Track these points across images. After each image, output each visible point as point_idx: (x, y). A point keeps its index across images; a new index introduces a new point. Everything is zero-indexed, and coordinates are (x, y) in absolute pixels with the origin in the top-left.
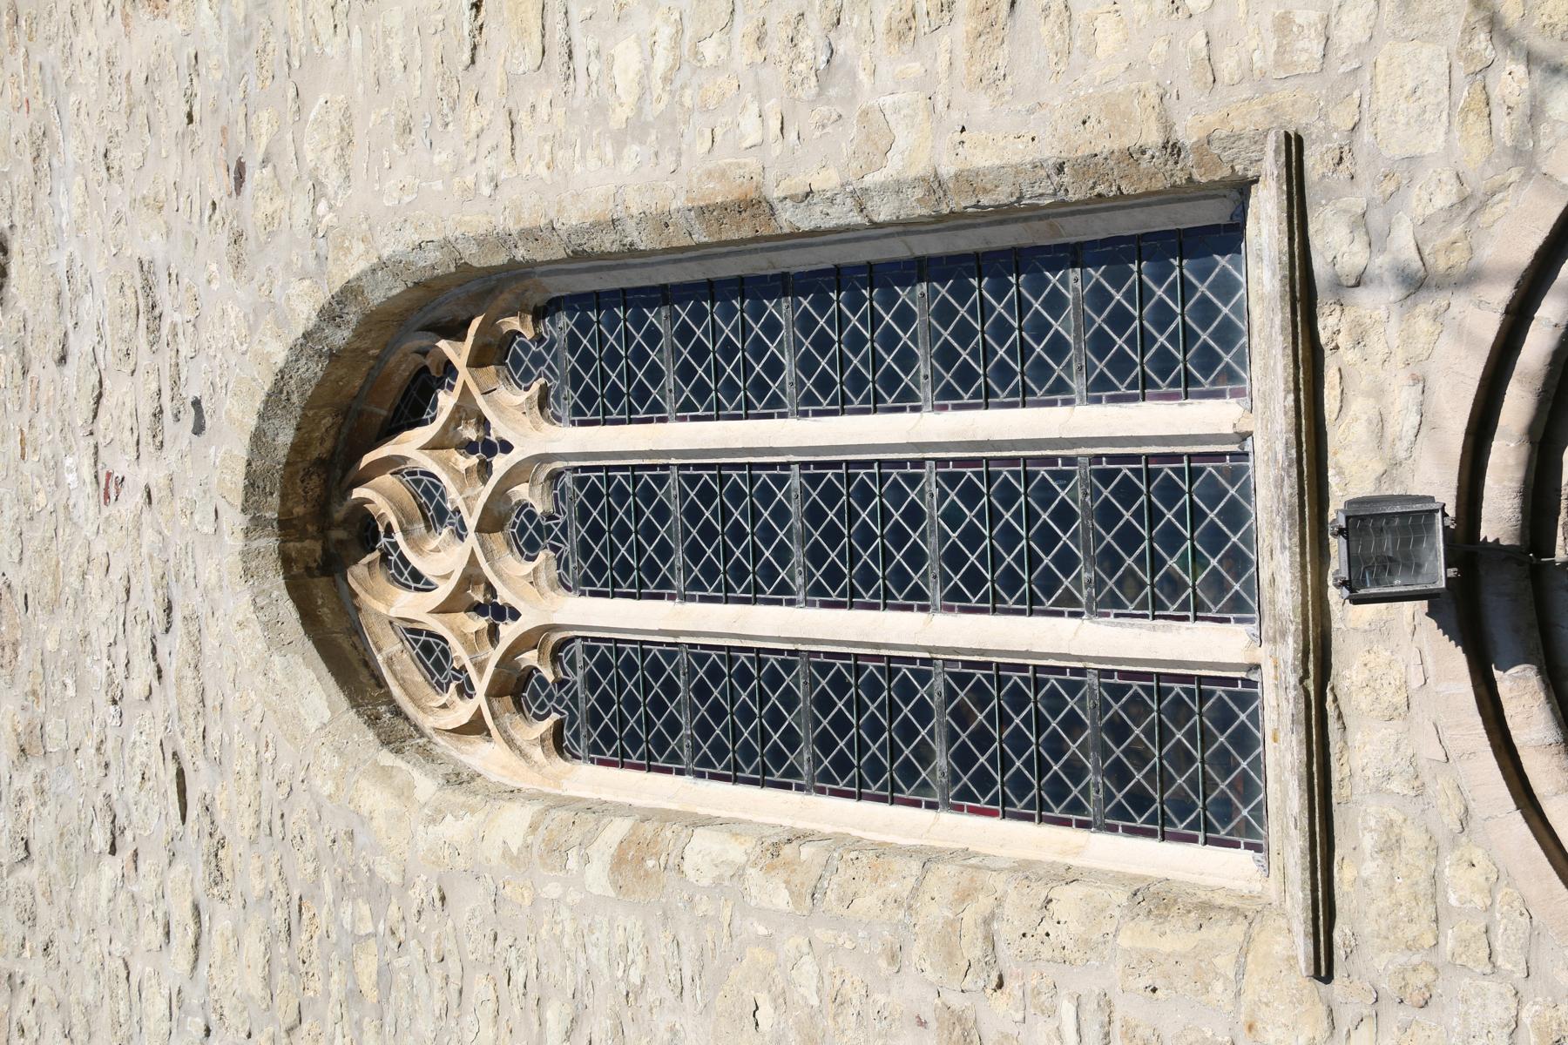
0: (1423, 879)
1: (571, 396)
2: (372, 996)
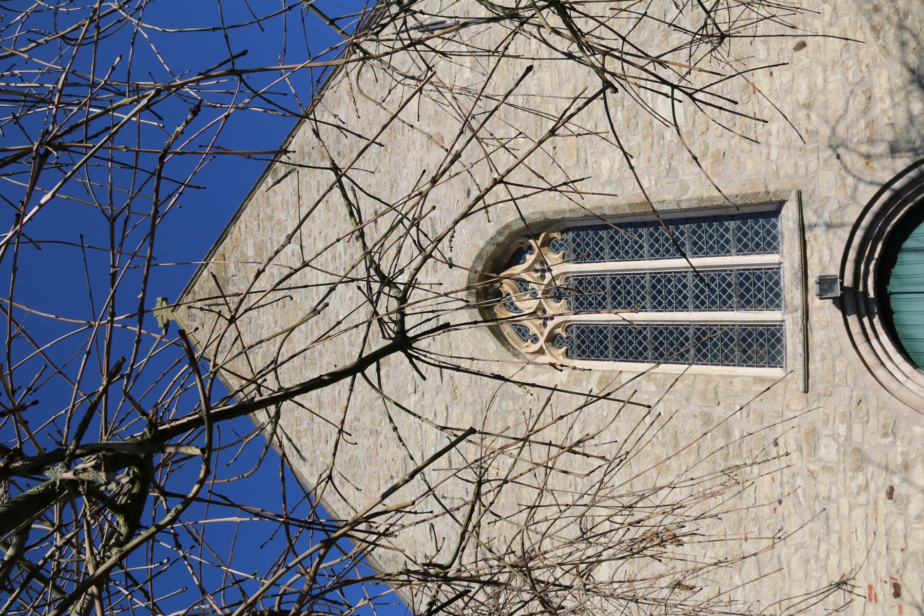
0: (830, 365)
1: (573, 256)
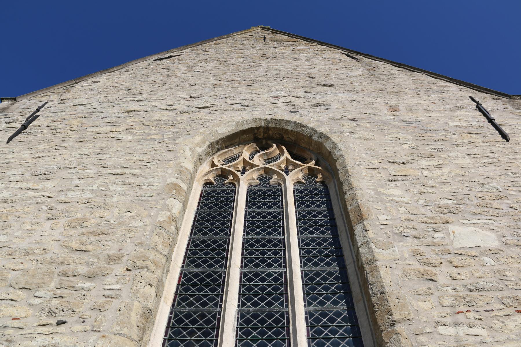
2: (149, 138)
